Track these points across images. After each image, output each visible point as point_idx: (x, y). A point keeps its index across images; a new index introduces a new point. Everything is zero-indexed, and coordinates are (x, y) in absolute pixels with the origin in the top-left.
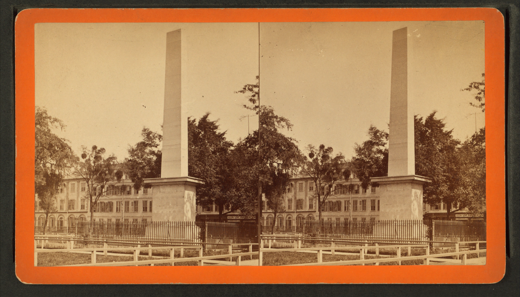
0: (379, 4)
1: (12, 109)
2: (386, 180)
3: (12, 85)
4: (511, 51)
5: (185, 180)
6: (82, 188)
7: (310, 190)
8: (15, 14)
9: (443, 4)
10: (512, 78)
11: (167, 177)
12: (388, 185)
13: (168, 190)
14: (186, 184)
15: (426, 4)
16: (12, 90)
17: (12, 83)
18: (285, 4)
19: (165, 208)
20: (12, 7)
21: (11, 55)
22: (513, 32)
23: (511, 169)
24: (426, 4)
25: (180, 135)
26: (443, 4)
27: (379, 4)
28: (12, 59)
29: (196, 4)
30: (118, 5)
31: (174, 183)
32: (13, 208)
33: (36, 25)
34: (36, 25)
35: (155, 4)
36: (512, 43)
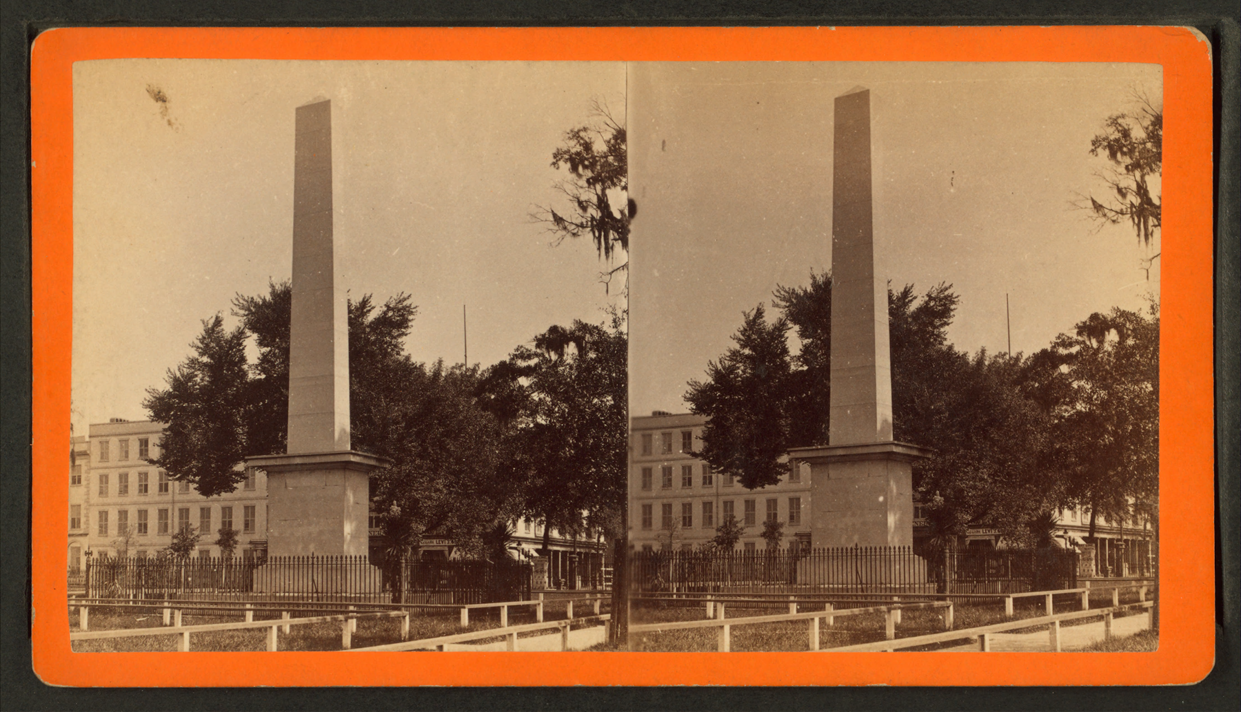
0: (907, 17)
1: (25, 269)
2: (285, 462)
3: (25, 213)
4: (1225, 128)
5: (888, 449)
6: (74, 478)
7: (74, 482)
8: (32, 37)
9: (1062, 16)
10: (1227, 196)
11: (301, 452)
12: (287, 475)
13: (308, 481)
14: (346, 467)
15: (1021, 16)
16: (25, 223)
17: (25, 206)
18: (681, 17)
19: (300, 525)
20: (25, 24)
21: (24, 141)
22: (1228, 85)
23: (1225, 414)
24: (1021, 16)
25: (331, 352)
26: (1062, 16)
27: (907, 17)
28: (24, 150)
29: (468, 18)
30: (281, 19)
31: (857, 457)
32: (27, 508)
33: (77, 66)
34: (77, 66)
35: (368, 18)
36: (1226, 111)
